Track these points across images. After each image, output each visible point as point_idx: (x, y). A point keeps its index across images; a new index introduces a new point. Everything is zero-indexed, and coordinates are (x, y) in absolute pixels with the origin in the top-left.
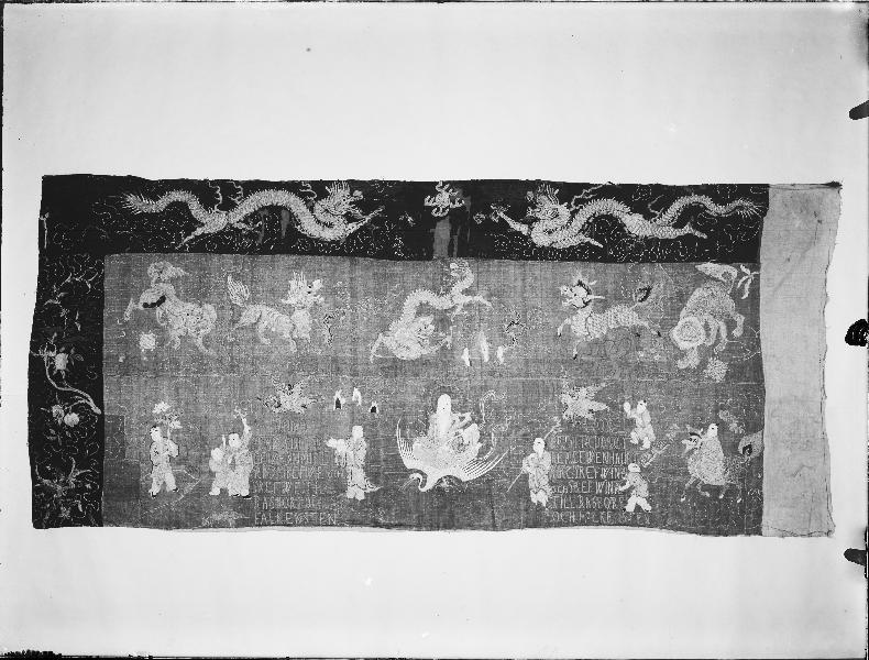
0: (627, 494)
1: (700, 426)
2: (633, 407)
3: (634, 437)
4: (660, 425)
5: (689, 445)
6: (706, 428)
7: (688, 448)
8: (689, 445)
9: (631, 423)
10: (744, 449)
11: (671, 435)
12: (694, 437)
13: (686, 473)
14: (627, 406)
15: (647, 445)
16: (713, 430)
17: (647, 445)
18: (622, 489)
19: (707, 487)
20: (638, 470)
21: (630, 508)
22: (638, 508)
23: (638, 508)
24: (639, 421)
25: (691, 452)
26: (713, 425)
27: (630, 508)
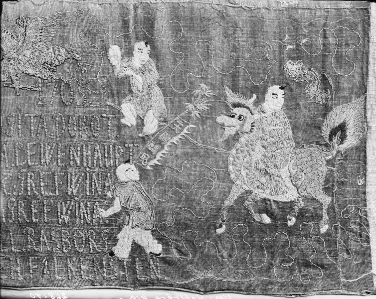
0: (115, 224)
1: (254, 90)
2: (128, 52)
3: (129, 112)
4: (177, 92)
5: (231, 125)
6: (260, 93)
7: (229, 132)
8: (231, 125)
9: (120, 88)
10: (333, 133)
11: (196, 108)
12: (237, 111)
13: (226, 177)
14: (115, 52)
15: (151, 127)
16: (275, 99)
17: (151, 127)
18: (106, 214)
19: (265, 206)
20: (135, 175)
21: (123, 251)
22: (137, 249)
23: (137, 249)
24: (138, 81)
25: (236, 137)
26: (275, 89)
27: (123, 251)
